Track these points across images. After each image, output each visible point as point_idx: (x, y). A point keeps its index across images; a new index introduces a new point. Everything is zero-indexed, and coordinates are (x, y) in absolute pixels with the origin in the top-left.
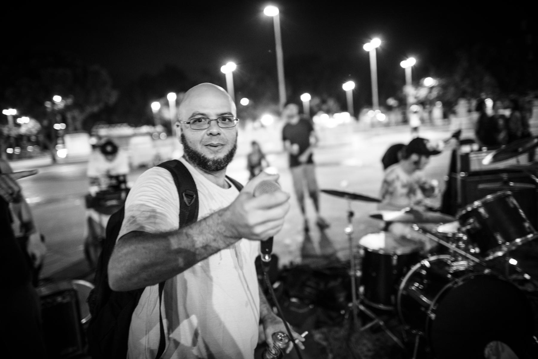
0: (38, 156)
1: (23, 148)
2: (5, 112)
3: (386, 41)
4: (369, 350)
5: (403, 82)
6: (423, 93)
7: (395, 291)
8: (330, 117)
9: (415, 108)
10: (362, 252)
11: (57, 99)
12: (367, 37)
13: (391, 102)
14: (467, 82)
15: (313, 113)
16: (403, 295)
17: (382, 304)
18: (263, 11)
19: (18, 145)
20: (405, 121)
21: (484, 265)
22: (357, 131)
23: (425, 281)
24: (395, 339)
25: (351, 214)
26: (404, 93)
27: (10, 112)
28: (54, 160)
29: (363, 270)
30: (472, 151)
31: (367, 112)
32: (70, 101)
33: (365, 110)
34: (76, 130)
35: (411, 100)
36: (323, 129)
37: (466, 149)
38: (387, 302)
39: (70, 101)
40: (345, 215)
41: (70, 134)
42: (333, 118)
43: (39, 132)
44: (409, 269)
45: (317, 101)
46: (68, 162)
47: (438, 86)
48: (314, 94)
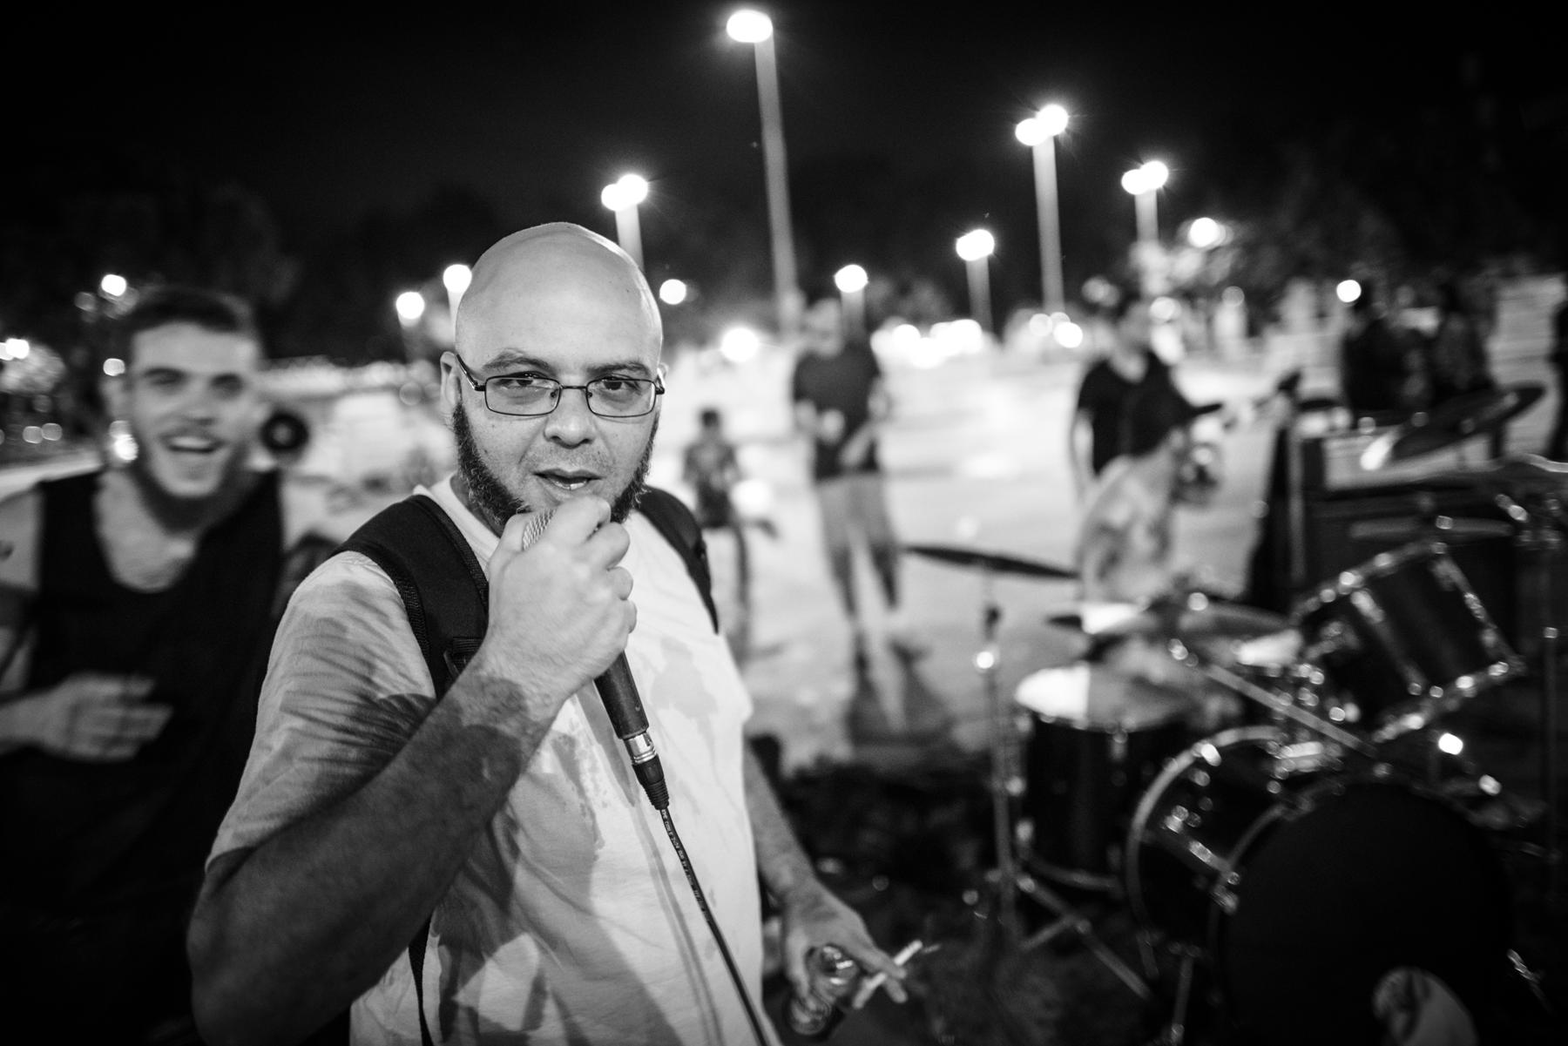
6: (1187, 265)
7: (1119, 834)
11: (114, 285)
12: (1024, 105)
13: (1099, 290)
15: (872, 321)
18: (725, 28)
25: (993, 616)
30: (1332, 429)
31: (1029, 318)
32: (151, 289)
33: (1021, 313)
35: (1154, 282)
37: (1313, 425)
38: (1099, 867)
39: (151, 289)
43: (59, 387)
44: (1158, 769)
47: (1233, 245)
48: (875, 267)
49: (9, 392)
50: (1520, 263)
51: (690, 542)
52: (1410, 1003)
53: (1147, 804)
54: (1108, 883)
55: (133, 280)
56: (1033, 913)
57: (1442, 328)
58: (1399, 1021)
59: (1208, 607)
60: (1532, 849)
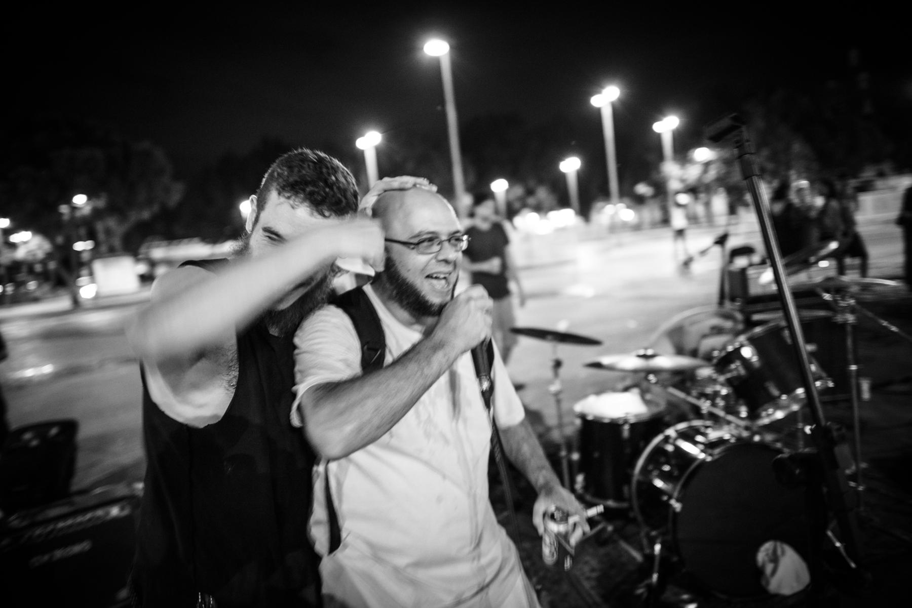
0: (48, 298)
1: (19, 284)
3: (628, 91)
4: (593, 570)
5: (661, 157)
6: (693, 173)
7: (628, 478)
8: (541, 218)
9: (683, 199)
10: (578, 422)
12: (594, 85)
13: (642, 189)
14: (765, 152)
15: (511, 212)
18: (423, 48)
19: (11, 280)
20: (666, 221)
22: (586, 238)
23: (673, 462)
25: (558, 364)
26: (662, 174)
28: (77, 303)
30: (751, 265)
31: (603, 207)
33: (599, 205)
34: (112, 252)
35: (674, 185)
36: (528, 238)
37: (741, 262)
38: (619, 497)
39: (101, 203)
40: (551, 364)
43: (49, 256)
44: (648, 442)
45: (519, 191)
46: (100, 305)
48: (513, 177)
50: (886, 167)
51: (487, 397)
52: (775, 559)
53: (641, 462)
55: (90, 197)
58: (769, 568)
59: (494, 303)
60: (852, 484)
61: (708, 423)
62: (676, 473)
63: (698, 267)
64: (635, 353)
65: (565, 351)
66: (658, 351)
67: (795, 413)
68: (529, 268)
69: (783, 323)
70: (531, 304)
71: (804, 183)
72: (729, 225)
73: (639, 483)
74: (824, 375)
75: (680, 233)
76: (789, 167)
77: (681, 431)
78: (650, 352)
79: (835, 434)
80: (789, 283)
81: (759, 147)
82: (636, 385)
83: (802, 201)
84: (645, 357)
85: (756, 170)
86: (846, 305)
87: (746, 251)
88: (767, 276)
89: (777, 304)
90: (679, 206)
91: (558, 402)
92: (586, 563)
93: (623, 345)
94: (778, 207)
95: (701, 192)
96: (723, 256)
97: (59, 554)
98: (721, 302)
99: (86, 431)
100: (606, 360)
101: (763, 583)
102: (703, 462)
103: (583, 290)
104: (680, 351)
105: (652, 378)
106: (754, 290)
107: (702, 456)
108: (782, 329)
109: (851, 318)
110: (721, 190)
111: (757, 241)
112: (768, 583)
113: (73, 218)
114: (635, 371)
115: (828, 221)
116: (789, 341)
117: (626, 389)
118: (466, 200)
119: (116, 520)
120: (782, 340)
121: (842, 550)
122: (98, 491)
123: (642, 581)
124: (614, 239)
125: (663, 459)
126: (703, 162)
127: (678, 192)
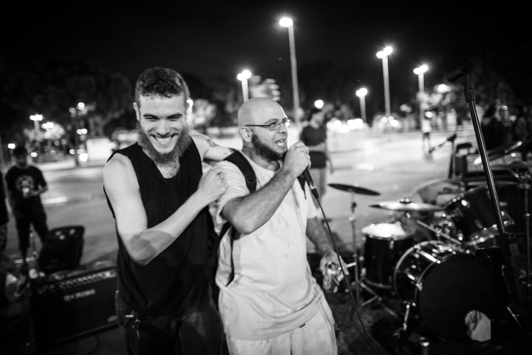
2: (32, 118)
5: (417, 89)
6: (436, 99)
7: (392, 272)
9: (429, 114)
10: (364, 239)
11: (81, 105)
12: (379, 45)
13: (405, 108)
15: (326, 120)
16: (398, 274)
17: (381, 284)
18: (279, 21)
20: (418, 127)
21: (466, 247)
22: (370, 136)
23: (418, 263)
24: (392, 313)
25: (354, 205)
26: (418, 100)
27: (36, 118)
28: (77, 163)
29: (365, 256)
30: (469, 154)
31: (381, 118)
32: (92, 108)
33: (378, 117)
34: (98, 135)
35: (424, 106)
36: (335, 135)
37: (463, 152)
38: (385, 282)
39: (92, 108)
40: (349, 205)
41: (92, 139)
42: (347, 124)
43: (63, 137)
44: (404, 252)
45: (330, 107)
46: (90, 165)
47: (452, 92)
48: (327, 99)
49: (47, 139)
52: (475, 321)
53: (399, 263)
54: (389, 287)
55: (86, 104)
56: (365, 295)
57: (517, 120)
58: (472, 325)
60: (524, 283)
61: (440, 242)
62: (420, 270)
63: (436, 155)
64: (399, 201)
65: (359, 198)
66: (412, 200)
67: (492, 239)
68: (335, 152)
69: (487, 187)
70: (337, 173)
71: (505, 107)
72: (456, 131)
73: (398, 274)
74: (510, 218)
75: (427, 135)
76: (495, 98)
77: (423, 246)
78: (407, 200)
79: (510, 237)
80: (490, 164)
81: (476, 87)
82: (399, 220)
83: (503, 118)
84: (405, 203)
85: (474, 98)
86: (525, 178)
87: (467, 146)
88: (478, 161)
89: (485, 177)
90: (426, 118)
91: (354, 227)
92: (366, 318)
93: (392, 196)
94: (487, 121)
95: (440, 111)
96: (453, 148)
97: (79, 295)
98: (450, 176)
99: (88, 234)
100: (382, 204)
101: (468, 334)
102: (436, 264)
103: (366, 166)
104: (425, 201)
105: (409, 216)
106: (471, 169)
107: (434, 260)
108: (486, 190)
109: (527, 186)
110: (453, 110)
111: (474, 141)
112: (471, 334)
113: (77, 116)
114: (399, 210)
115: (518, 130)
116: (490, 197)
117: (393, 223)
118: (299, 112)
119: (108, 279)
120: (485, 196)
121: (516, 318)
122: (98, 263)
123: (398, 329)
124: (386, 137)
125: (412, 262)
126: (443, 93)
127: (426, 111)
